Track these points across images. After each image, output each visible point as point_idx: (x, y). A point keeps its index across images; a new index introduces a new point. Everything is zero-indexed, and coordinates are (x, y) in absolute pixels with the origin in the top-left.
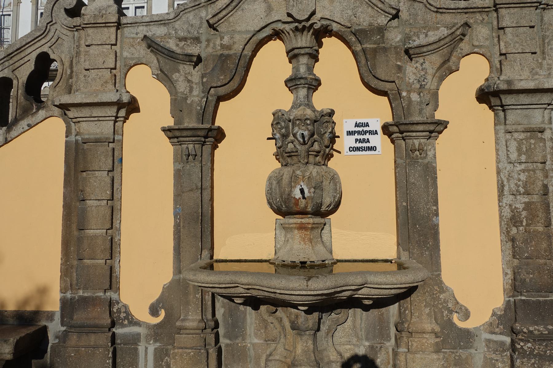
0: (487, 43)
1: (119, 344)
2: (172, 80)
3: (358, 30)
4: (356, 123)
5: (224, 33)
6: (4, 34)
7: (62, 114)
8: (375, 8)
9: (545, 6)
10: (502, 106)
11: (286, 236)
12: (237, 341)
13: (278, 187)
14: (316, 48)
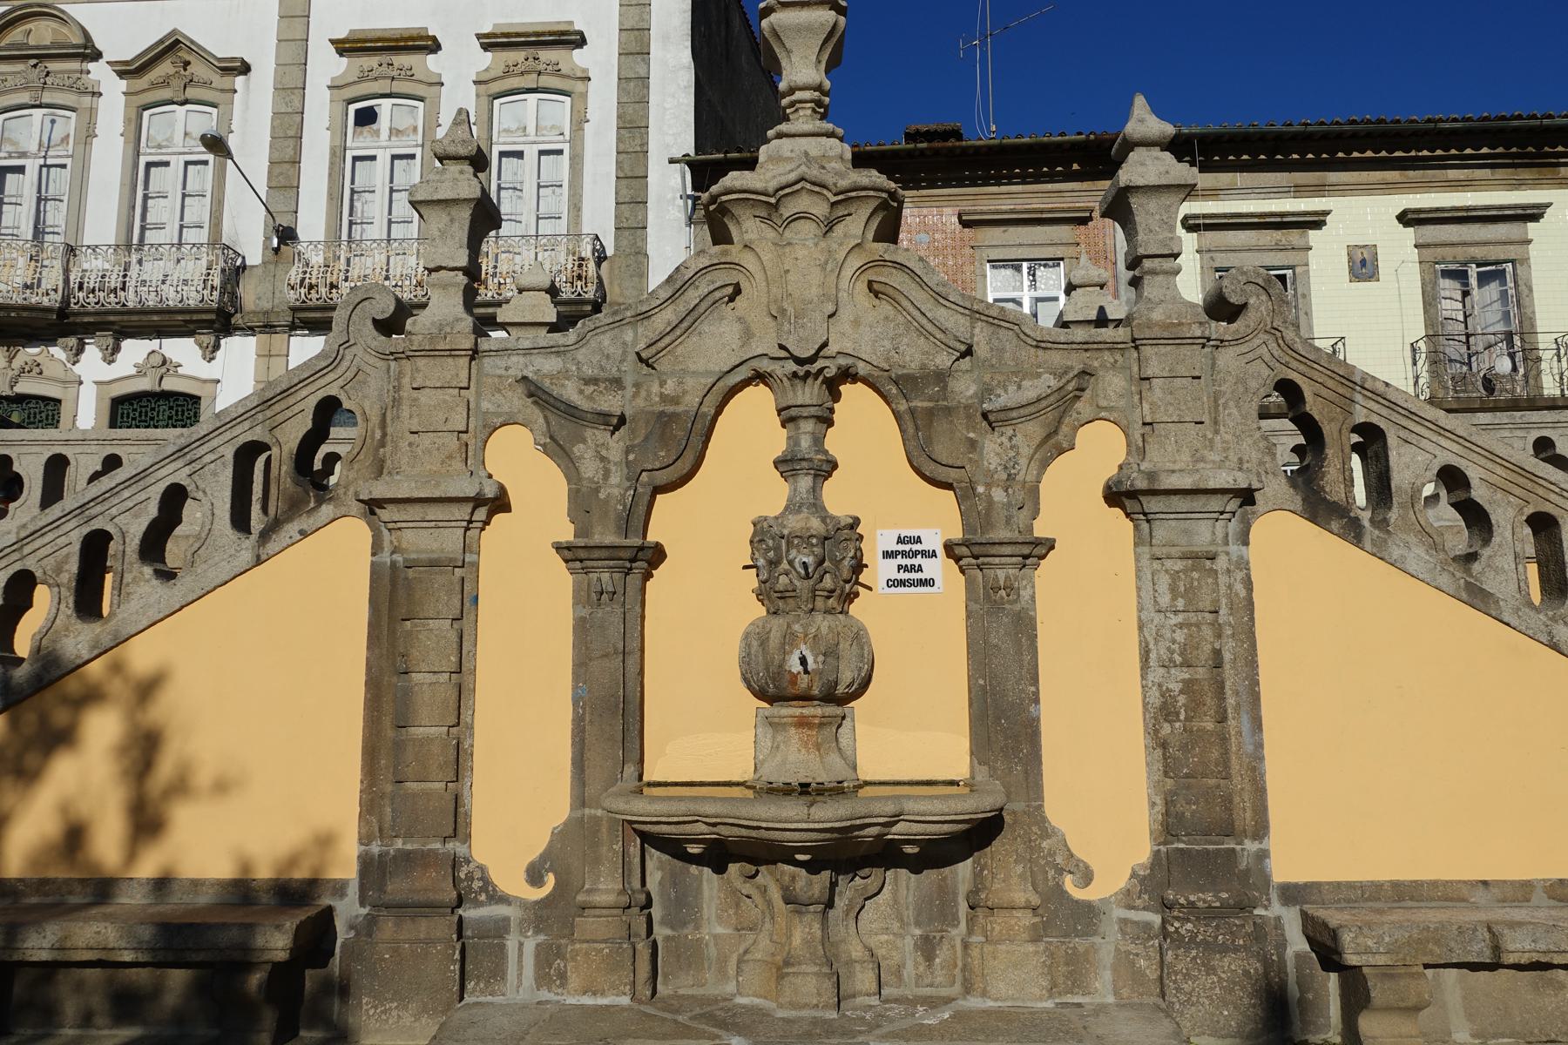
0: (1122, 403)
1: (469, 938)
2: (572, 456)
4: (899, 537)
5: (665, 374)
7: (365, 512)
8: (932, 338)
9: (1218, 343)
10: (1145, 514)
11: (774, 738)
12: (686, 931)
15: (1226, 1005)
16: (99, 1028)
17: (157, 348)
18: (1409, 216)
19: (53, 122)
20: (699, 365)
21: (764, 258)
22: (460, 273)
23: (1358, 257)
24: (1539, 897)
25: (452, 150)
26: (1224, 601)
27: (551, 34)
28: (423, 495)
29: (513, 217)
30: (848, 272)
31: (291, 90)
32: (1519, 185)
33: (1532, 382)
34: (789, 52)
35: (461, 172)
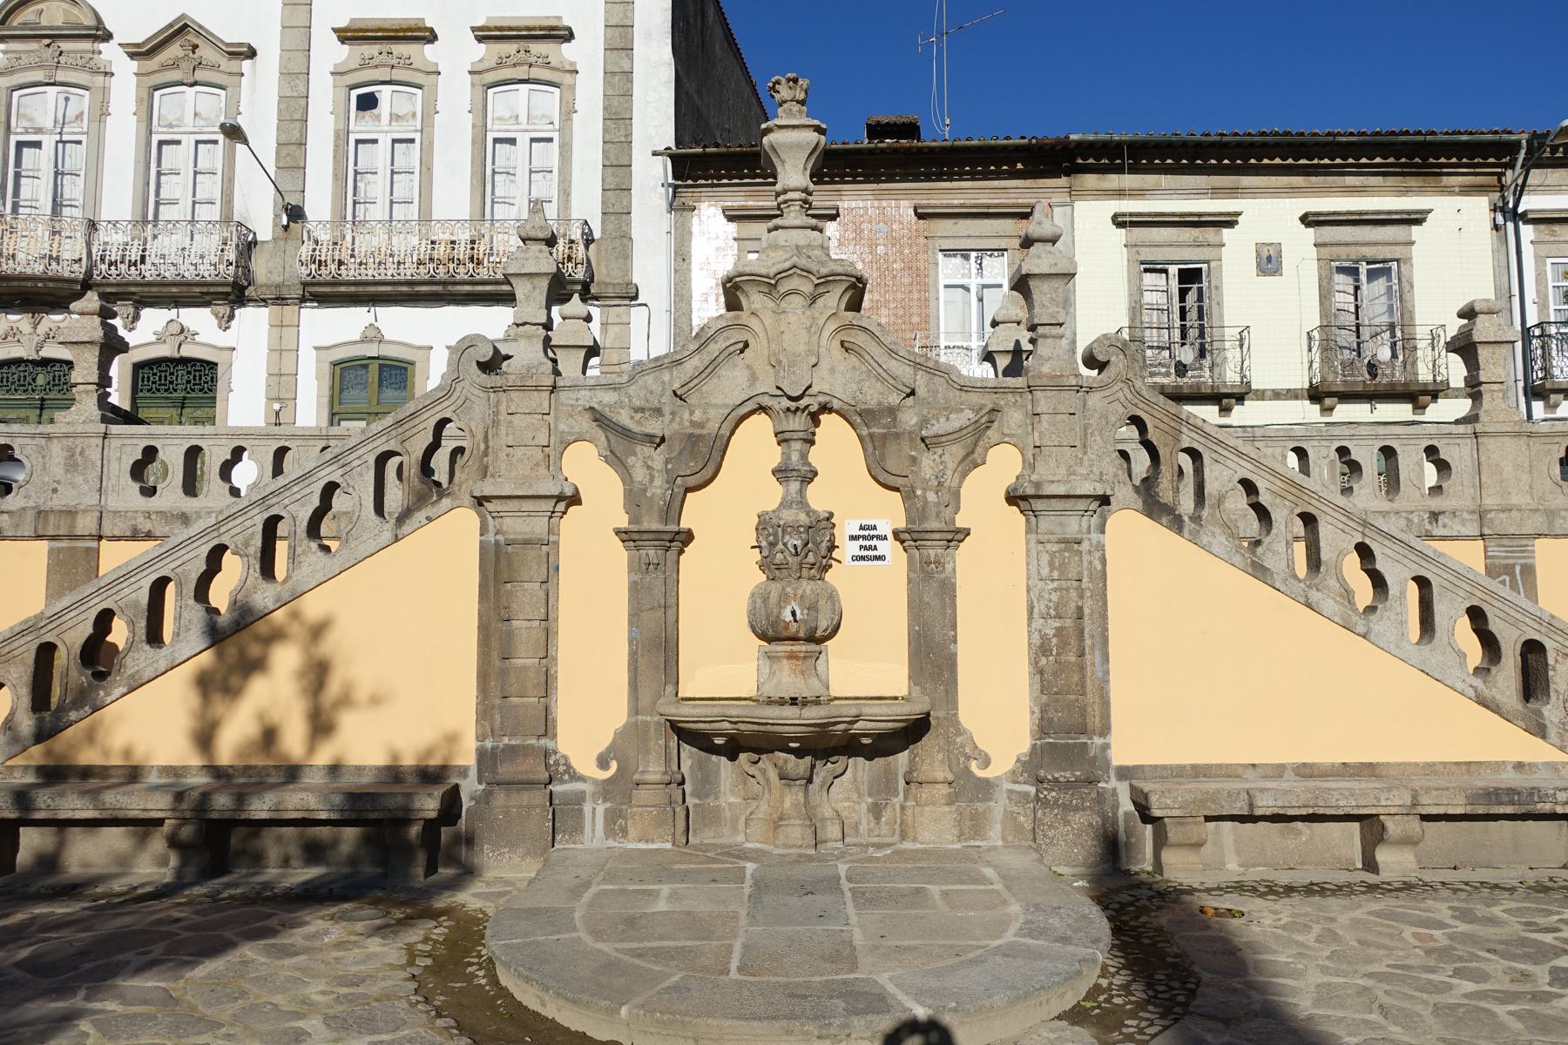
0: (1020, 431)
3: (864, 410)
6: (65, 188)
11: (771, 666)
12: (708, 801)
15: (1076, 845)
16: (293, 868)
17: (175, 317)
18: (1310, 219)
19: (67, 99)
20: (717, 399)
21: (766, 323)
22: (541, 327)
23: (1265, 254)
24: (1289, 774)
25: (533, 234)
26: (1086, 573)
27: (541, 29)
28: (520, 494)
29: (507, 200)
30: (826, 334)
31: (296, 75)
32: (1406, 192)
33: (1408, 367)
34: (783, 162)
35: (540, 251)
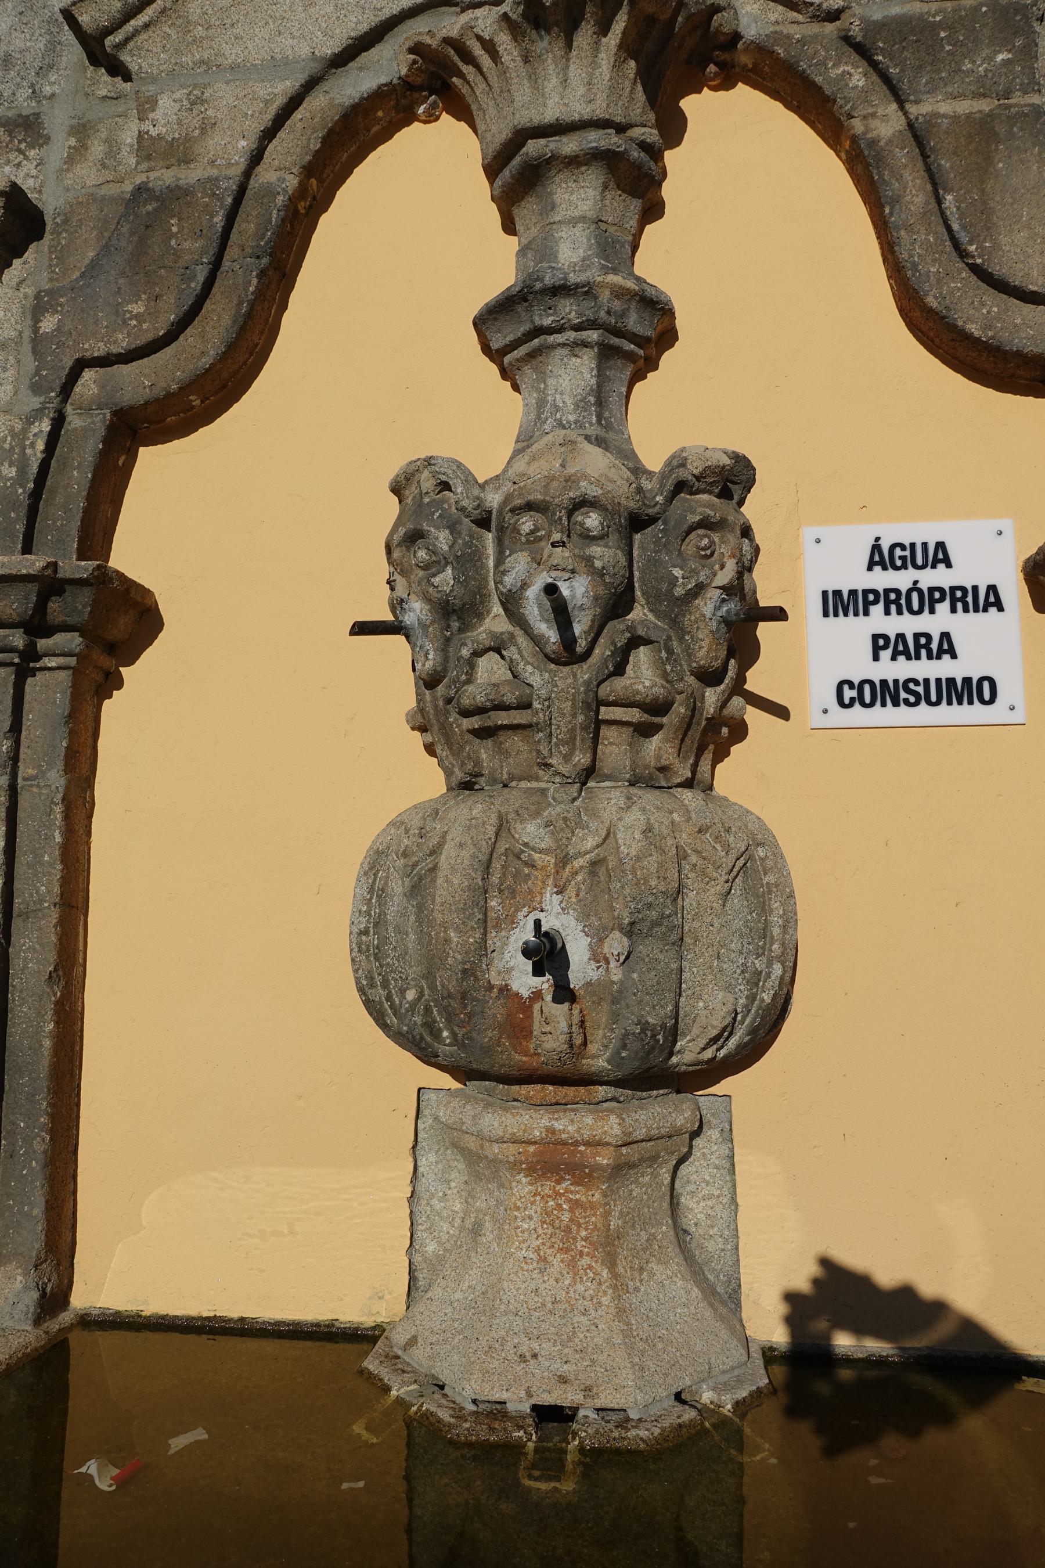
3: (883, 25)
4: (876, 548)
5: (154, 79)
13: (413, 918)
14: (652, 135)
